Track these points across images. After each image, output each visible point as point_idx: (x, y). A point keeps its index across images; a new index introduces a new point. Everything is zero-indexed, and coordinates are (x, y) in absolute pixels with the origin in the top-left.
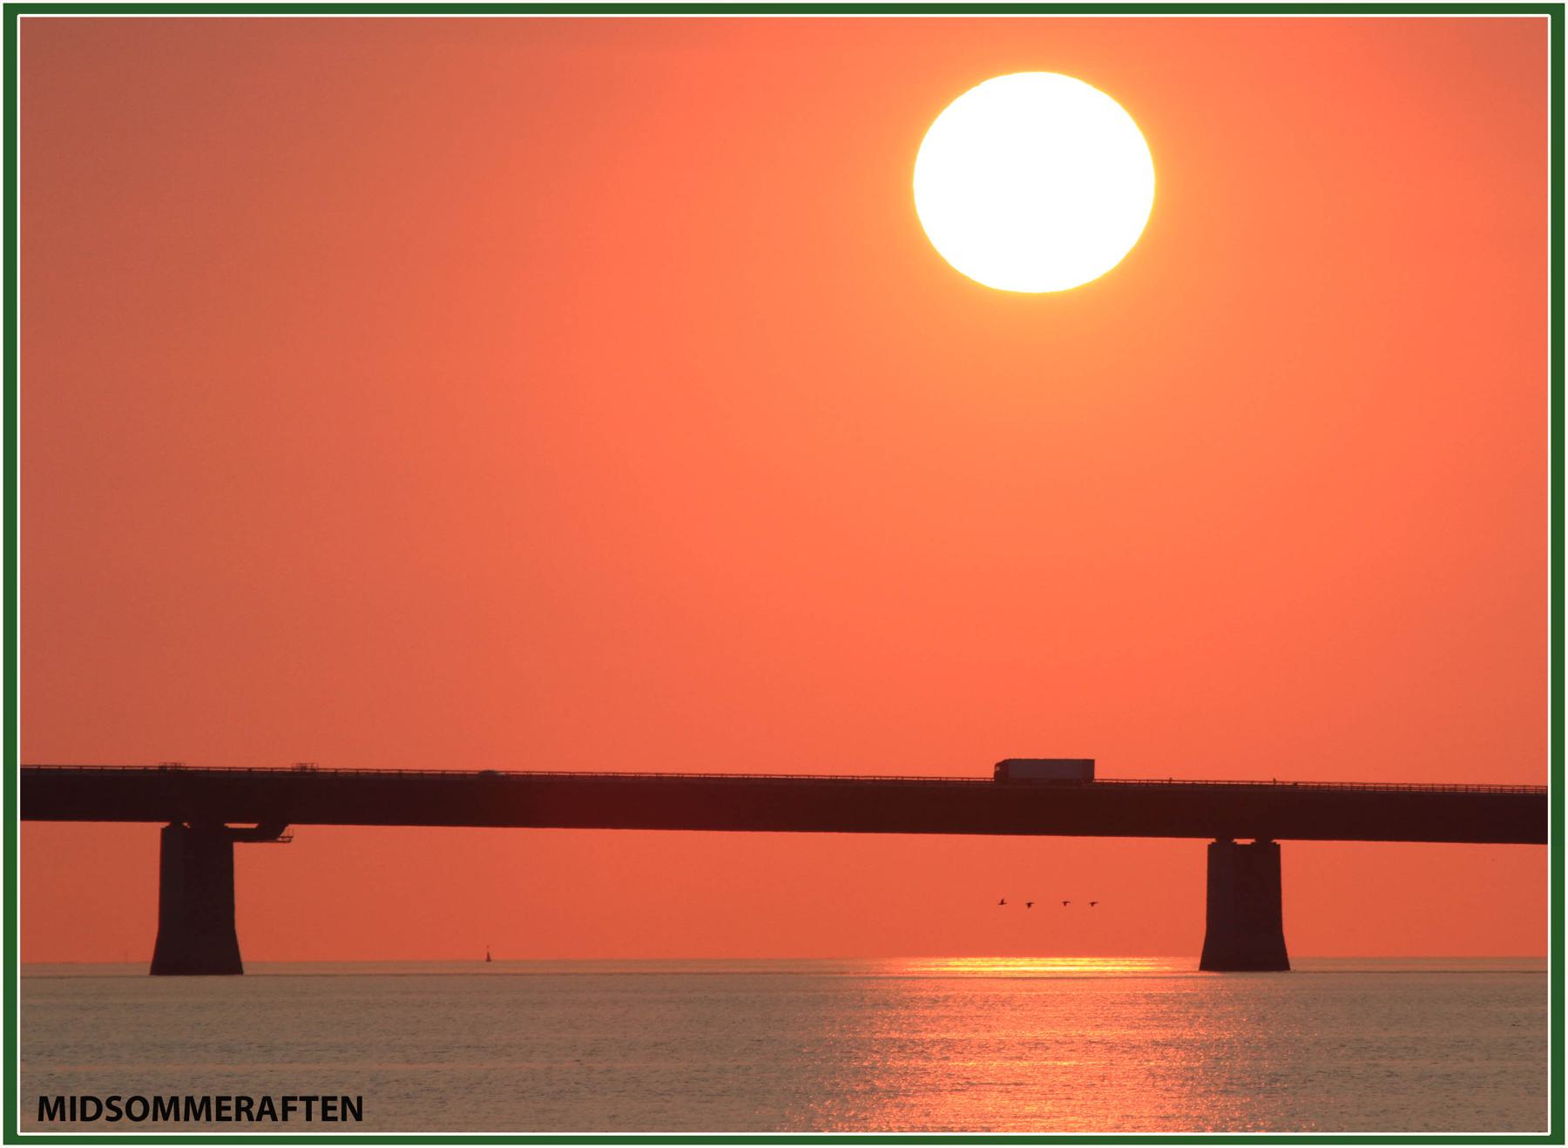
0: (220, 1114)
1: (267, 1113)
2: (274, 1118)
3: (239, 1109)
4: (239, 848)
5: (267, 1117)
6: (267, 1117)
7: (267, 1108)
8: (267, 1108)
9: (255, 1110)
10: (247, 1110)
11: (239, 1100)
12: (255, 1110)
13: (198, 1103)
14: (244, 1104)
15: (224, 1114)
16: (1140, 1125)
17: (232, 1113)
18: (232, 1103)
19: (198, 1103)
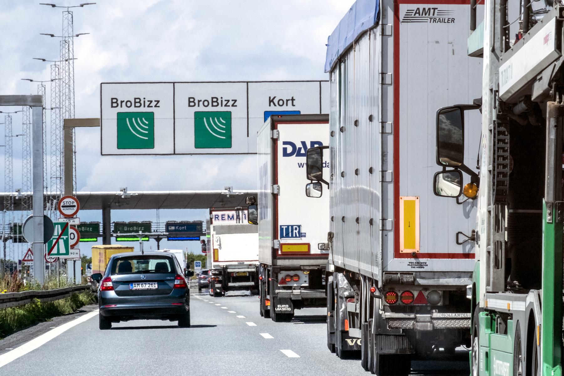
0: (168, 228)
1: (417, 13)
2: (440, 22)
3: (452, 21)
4: (154, 269)
5: (439, 22)
6: (439, 22)
7: (418, 12)
8: (418, 12)
9: (437, 21)
10: (435, 21)
11: (452, 19)
12: (437, 21)
13: (301, 166)
14: (453, 20)
15: (449, 21)
16: (338, 239)
17: (450, 21)
18: (451, 20)
19: (301, 166)
